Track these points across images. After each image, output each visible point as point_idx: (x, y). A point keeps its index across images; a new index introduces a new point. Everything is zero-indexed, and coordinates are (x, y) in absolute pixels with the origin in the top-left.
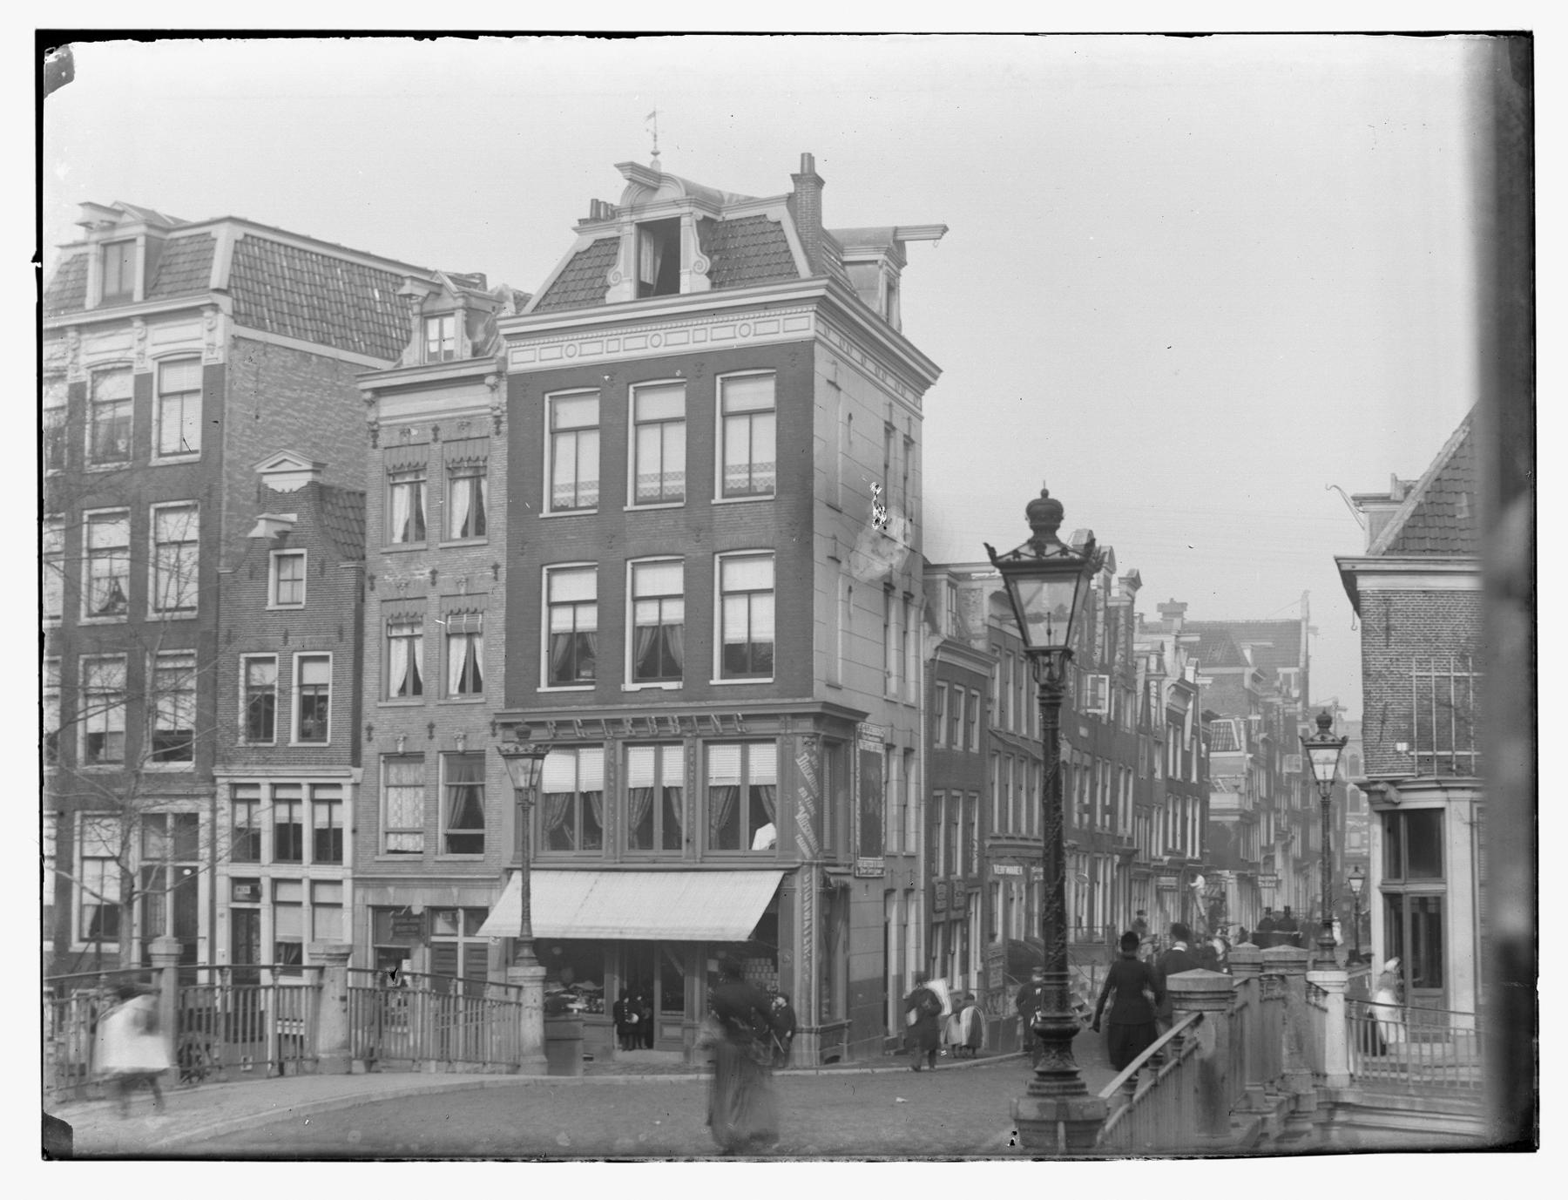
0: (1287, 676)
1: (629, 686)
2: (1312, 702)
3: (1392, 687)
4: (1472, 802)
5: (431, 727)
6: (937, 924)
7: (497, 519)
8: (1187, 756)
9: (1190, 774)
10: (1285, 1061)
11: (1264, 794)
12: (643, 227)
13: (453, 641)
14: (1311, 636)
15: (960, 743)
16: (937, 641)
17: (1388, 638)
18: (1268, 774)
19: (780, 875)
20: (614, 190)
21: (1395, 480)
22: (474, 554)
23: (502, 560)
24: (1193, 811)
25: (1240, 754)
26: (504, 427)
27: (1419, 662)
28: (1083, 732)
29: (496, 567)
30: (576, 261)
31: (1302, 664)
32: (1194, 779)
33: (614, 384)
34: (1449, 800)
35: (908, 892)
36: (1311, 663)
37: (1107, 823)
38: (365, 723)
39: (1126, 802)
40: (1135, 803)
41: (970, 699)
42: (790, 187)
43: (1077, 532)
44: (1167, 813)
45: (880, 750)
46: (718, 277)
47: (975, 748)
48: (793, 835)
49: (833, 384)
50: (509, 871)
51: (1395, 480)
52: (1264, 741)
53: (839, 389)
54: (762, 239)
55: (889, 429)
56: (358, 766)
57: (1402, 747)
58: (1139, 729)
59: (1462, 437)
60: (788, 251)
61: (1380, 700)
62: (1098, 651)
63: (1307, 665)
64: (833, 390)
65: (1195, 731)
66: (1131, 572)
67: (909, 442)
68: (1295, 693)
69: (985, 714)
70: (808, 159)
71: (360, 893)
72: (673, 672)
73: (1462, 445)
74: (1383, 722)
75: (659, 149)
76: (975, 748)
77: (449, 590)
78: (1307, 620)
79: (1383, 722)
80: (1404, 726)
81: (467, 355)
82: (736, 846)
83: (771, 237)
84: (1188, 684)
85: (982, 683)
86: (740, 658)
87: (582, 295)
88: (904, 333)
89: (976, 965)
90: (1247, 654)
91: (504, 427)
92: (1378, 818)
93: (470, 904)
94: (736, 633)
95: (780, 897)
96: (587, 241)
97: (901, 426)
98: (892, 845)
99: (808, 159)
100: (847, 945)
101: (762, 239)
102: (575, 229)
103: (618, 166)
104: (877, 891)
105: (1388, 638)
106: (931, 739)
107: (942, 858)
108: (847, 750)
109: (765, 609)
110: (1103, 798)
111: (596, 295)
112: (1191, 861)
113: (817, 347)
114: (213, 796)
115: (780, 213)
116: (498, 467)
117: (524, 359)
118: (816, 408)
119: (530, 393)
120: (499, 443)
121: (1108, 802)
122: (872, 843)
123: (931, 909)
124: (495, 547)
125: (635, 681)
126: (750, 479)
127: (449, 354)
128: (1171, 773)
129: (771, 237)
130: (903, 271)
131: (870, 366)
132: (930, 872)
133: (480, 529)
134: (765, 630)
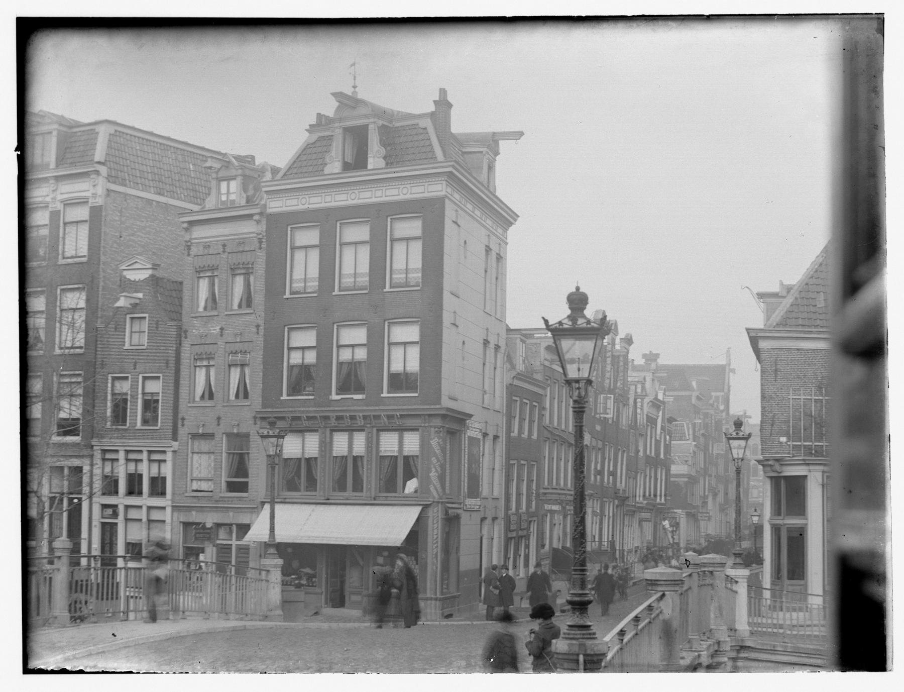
0: (717, 398)
2: (731, 412)
4: (823, 472)
5: (219, 419)
6: (511, 538)
7: (259, 299)
8: (658, 443)
10: (712, 622)
12: (346, 130)
15: (526, 433)
16: (514, 373)
18: (705, 454)
19: (420, 508)
20: (330, 108)
21: (782, 284)
22: (247, 318)
23: (261, 323)
24: (661, 474)
25: (689, 442)
26: (264, 245)
29: (258, 326)
31: (726, 391)
32: (662, 456)
33: (328, 221)
35: (494, 519)
36: (731, 388)
38: (180, 416)
39: (621, 470)
40: (627, 470)
41: (533, 408)
44: (645, 476)
45: (480, 437)
46: (390, 160)
47: (535, 436)
49: (456, 223)
50: (263, 503)
51: (782, 284)
52: (703, 435)
53: (459, 226)
55: (488, 250)
56: (176, 440)
57: (783, 439)
58: (630, 427)
59: (821, 260)
60: (431, 145)
61: (771, 412)
62: (607, 381)
63: (729, 391)
64: (456, 226)
65: (663, 428)
66: (627, 335)
67: (499, 258)
68: (722, 407)
69: (541, 416)
70: (443, 92)
71: (176, 514)
72: (360, 389)
74: (772, 425)
76: (535, 436)
77: (230, 339)
78: (729, 364)
81: (243, 202)
83: (421, 137)
84: (659, 401)
85: (539, 398)
87: (310, 169)
90: (694, 384)
91: (264, 245)
92: (768, 482)
94: (397, 367)
95: (420, 521)
96: (315, 137)
97: (495, 248)
98: (485, 491)
99: (443, 92)
100: (458, 549)
102: (307, 130)
104: (477, 517)
106: (509, 430)
108: (460, 436)
109: (414, 353)
110: (608, 466)
111: (318, 169)
113: (447, 201)
114: (92, 457)
115: (427, 123)
116: (260, 269)
117: (276, 206)
118: (446, 238)
119: (279, 226)
121: (611, 469)
122: (474, 492)
123: (508, 529)
124: (258, 314)
126: (406, 278)
127: (233, 202)
128: (648, 452)
129: (421, 137)
131: (478, 212)
132: (507, 507)
134: (413, 365)
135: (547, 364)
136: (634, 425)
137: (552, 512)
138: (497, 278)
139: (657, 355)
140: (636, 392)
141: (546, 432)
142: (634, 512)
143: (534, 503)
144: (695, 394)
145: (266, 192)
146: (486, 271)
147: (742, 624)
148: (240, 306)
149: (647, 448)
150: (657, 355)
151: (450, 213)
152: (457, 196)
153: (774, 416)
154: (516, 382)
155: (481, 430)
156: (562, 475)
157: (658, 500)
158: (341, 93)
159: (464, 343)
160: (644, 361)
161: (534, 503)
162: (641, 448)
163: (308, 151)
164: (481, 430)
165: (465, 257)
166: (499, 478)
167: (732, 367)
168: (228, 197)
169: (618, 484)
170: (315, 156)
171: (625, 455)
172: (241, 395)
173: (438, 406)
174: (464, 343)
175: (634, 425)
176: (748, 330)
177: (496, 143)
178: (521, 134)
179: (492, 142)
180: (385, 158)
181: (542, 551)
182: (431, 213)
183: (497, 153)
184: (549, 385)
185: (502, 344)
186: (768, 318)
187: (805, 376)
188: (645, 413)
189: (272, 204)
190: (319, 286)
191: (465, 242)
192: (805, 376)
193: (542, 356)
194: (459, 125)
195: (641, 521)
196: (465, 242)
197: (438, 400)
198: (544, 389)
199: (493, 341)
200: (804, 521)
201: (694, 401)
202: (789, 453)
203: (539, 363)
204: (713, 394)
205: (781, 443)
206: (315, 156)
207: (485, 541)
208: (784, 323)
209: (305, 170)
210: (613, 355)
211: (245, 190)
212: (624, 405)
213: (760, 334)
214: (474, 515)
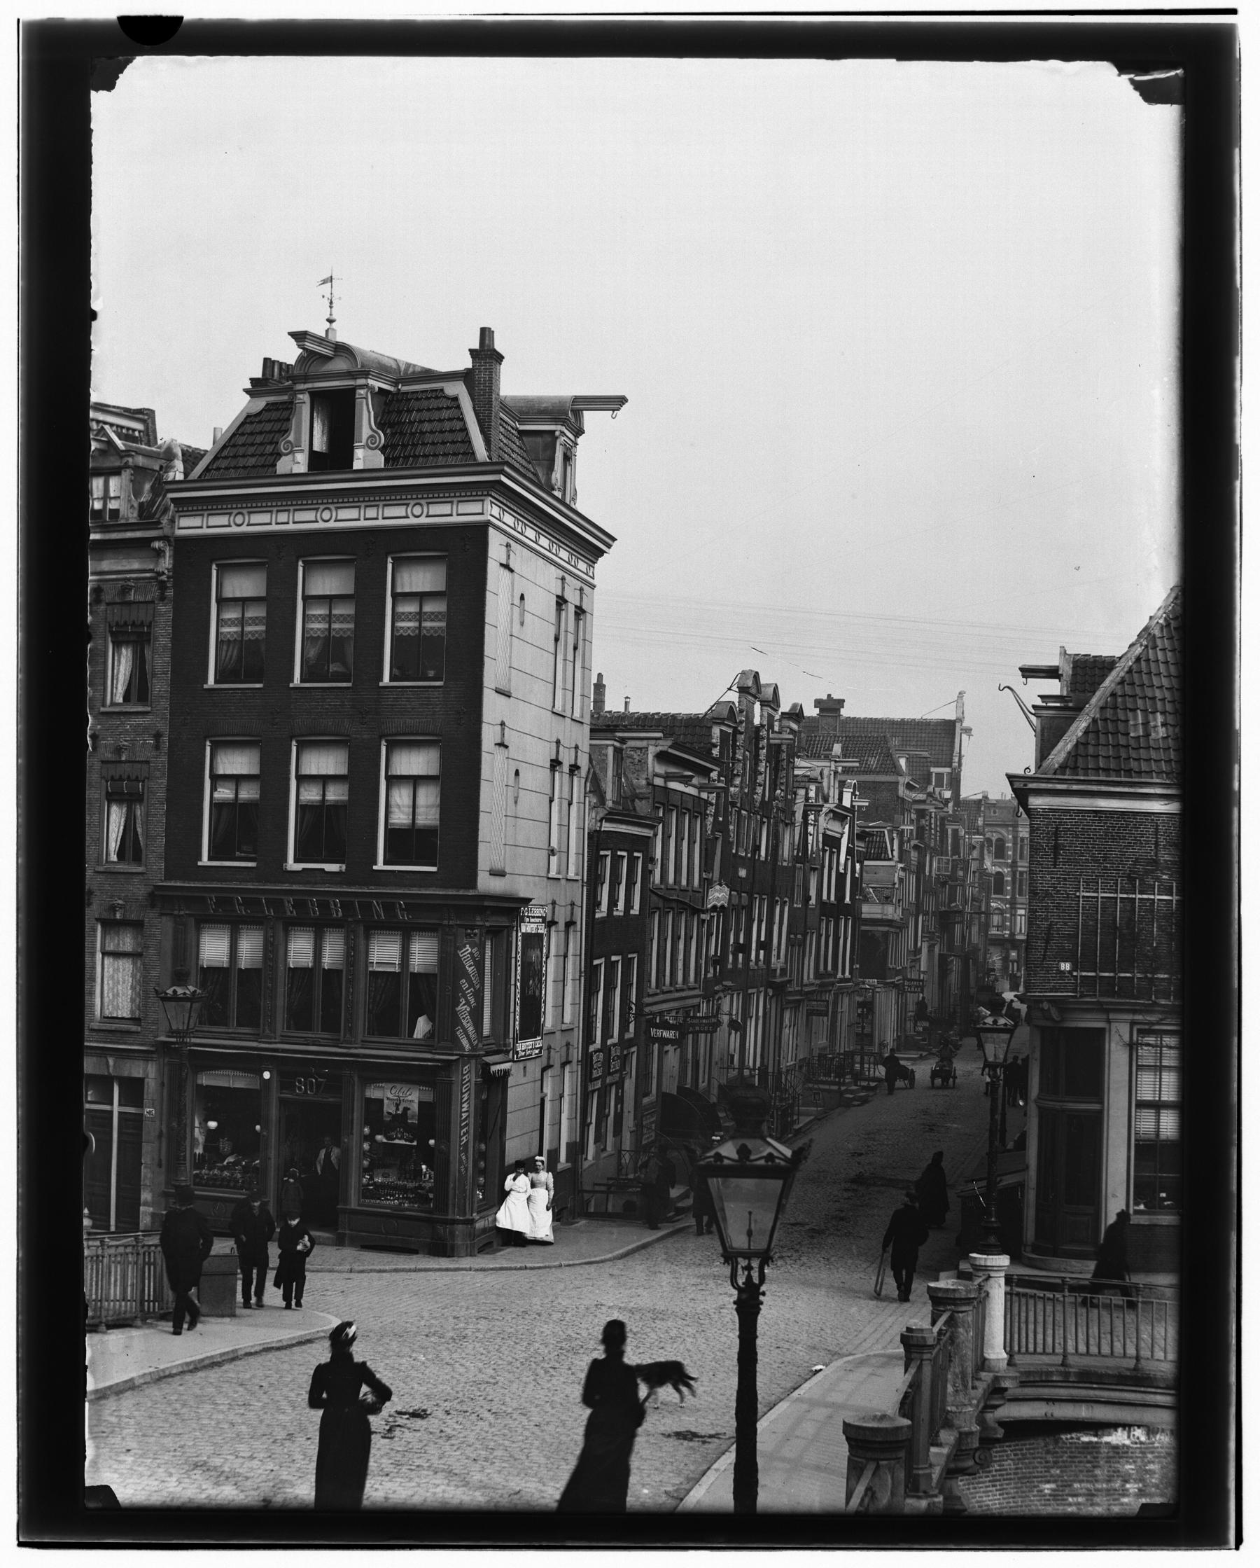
0: (940, 776)
1: (292, 865)
3: (1058, 906)
7: (160, 686)
8: (841, 878)
9: (844, 898)
10: (950, 1399)
11: (913, 898)
13: (122, 1468)
14: (964, 736)
17: (1056, 858)
20: (289, 354)
21: (1064, 653)
22: (140, 720)
23: (164, 728)
25: (892, 863)
26: (170, 593)
27: (1087, 882)
28: (743, 873)
29: (158, 736)
30: (248, 422)
32: (847, 900)
33: (278, 556)
34: (1109, 1021)
36: (963, 761)
37: (762, 957)
39: (780, 937)
40: (789, 933)
41: (632, 862)
42: (466, 363)
43: (743, 673)
44: (819, 936)
45: (542, 930)
46: (396, 455)
47: (636, 910)
48: (454, 1027)
49: (506, 566)
51: (1064, 653)
52: (916, 847)
53: (512, 571)
54: (436, 415)
55: (561, 601)
58: (796, 859)
59: (1139, 650)
60: (464, 429)
61: (1046, 919)
62: (759, 790)
63: (960, 764)
64: (507, 572)
66: (795, 706)
67: (580, 612)
69: (647, 873)
70: (486, 334)
73: (1138, 659)
74: (1047, 942)
75: (334, 317)
76: (636, 910)
77: (109, 756)
78: (960, 720)
79: (1047, 942)
80: (1068, 946)
81: (133, 517)
82: (396, 1034)
83: (445, 414)
84: (845, 809)
85: (644, 844)
86: (406, 842)
87: (252, 461)
88: (580, 506)
89: (629, 1122)
91: (170, 593)
93: (126, 1074)
96: (260, 404)
97: (572, 597)
98: (549, 1022)
99: (486, 334)
101: (436, 415)
102: (246, 391)
103: (290, 334)
104: (534, 1068)
105: (1056, 858)
106: (593, 903)
107: (599, 1025)
108: (510, 935)
109: (428, 798)
111: (266, 467)
112: (841, 981)
113: (491, 530)
115: (458, 389)
116: (163, 635)
117: (190, 526)
119: (199, 556)
120: (163, 609)
121: (763, 939)
122: (531, 1027)
123: (587, 1078)
124: (158, 716)
125: (296, 860)
127: (115, 513)
128: (825, 897)
129: (445, 414)
130: (580, 440)
131: (544, 541)
132: (588, 1037)
133: (143, 697)
135: (659, 782)
136: (802, 855)
137: (664, 1042)
138: (575, 648)
139: (841, 703)
140: (807, 798)
141: (654, 898)
142: (799, 1001)
143: (632, 1026)
144: (903, 780)
145: (173, 500)
146: (557, 639)
147: (996, 1351)
148: (127, 697)
149: (821, 888)
150: (841, 703)
151: (496, 547)
152: (509, 519)
153: (1050, 927)
154: (607, 826)
155: (544, 919)
156: (681, 957)
157: (840, 975)
158: (305, 333)
159: (517, 773)
160: (817, 711)
161: (632, 1026)
162: (813, 893)
163: (248, 428)
164: (544, 919)
165: (522, 624)
166: (572, 991)
167: (964, 725)
168: (105, 505)
169: (774, 959)
170: (259, 439)
171: (786, 909)
172: (129, 853)
173: (471, 893)
174: (517, 773)
175: (802, 855)
176: (1009, 777)
177: (578, 414)
178: (622, 400)
179: (570, 414)
180: (383, 450)
181: (646, 1100)
182: (464, 552)
183: (579, 432)
184: (660, 820)
185: (583, 762)
186: (1044, 751)
187: (1105, 858)
188: (821, 831)
189: (184, 522)
190: (267, 631)
191: (522, 597)
192: (1105, 858)
193: (650, 769)
194: (515, 382)
195: (810, 1013)
196: (522, 597)
197: (472, 881)
198: (652, 827)
199: (567, 759)
200: (1096, 1107)
201: (902, 791)
202: (1075, 991)
203: (644, 782)
204: (934, 770)
205: (1063, 972)
206: (259, 439)
207: (548, 1106)
208: (1072, 764)
209: (242, 462)
210: (769, 745)
211: (137, 493)
212: (787, 825)
213: (1031, 786)
214: (530, 1065)
